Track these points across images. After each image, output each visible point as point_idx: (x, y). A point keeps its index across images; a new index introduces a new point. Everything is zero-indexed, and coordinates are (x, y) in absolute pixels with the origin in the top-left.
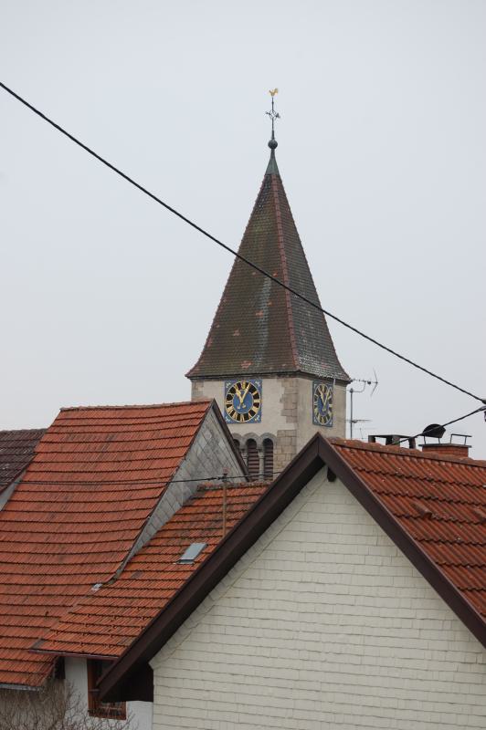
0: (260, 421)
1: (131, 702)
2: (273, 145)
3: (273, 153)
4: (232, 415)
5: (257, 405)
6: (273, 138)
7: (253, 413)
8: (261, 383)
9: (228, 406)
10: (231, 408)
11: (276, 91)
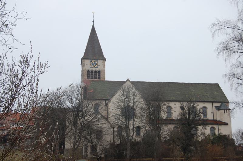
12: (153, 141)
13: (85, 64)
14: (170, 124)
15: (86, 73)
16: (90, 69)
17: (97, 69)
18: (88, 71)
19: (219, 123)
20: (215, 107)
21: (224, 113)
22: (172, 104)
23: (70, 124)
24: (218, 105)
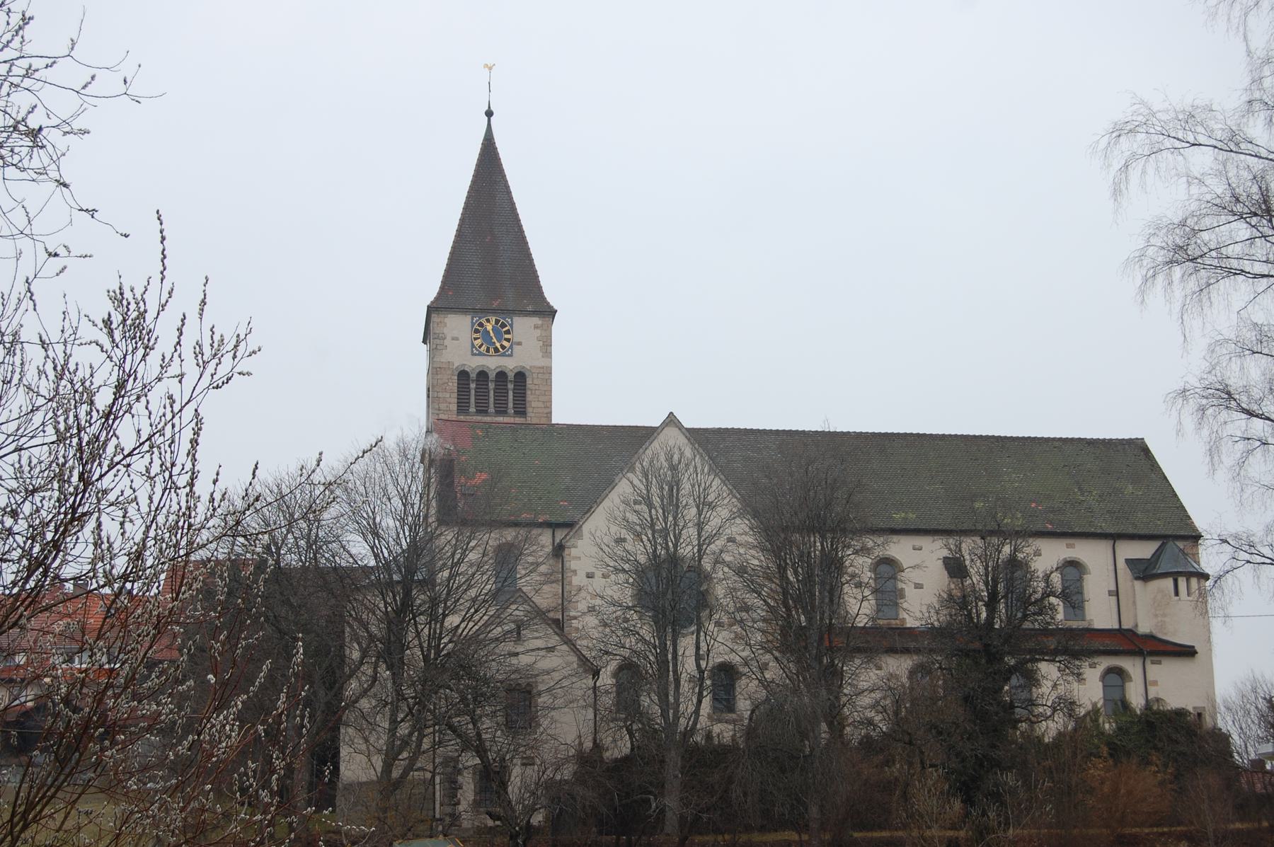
0: (473, 354)
1: (1109, 627)
2: (489, 114)
3: (489, 121)
4: (480, 347)
5: (508, 340)
6: (489, 107)
7: (503, 347)
8: (512, 321)
9: (475, 339)
10: (479, 340)
11: (486, 66)
15: (453, 385)
16: (475, 364)
18: (463, 375)
20: (1129, 562)
21: (1177, 594)
22: (901, 549)
23: (364, 653)
24: (1144, 550)
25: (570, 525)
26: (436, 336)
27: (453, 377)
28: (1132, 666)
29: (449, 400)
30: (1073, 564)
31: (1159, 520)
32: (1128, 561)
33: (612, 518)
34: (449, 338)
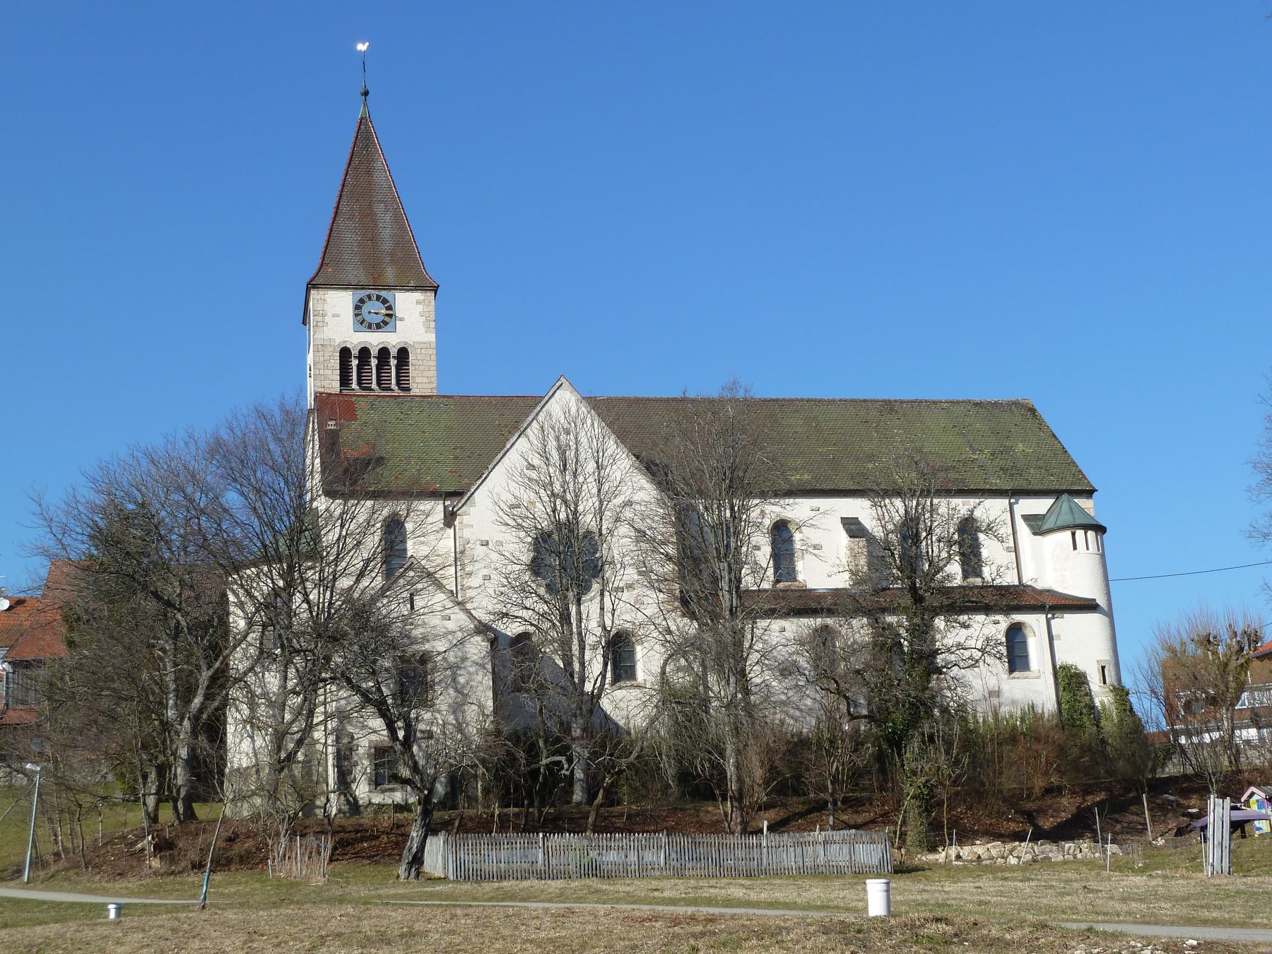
12: (276, 598)
13: (323, 316)
14: (987, 609)
15: (335, 362)
16: (357, 340)
17: (391, 339)
18: (345, 353)
19: (1049, 603)
20: (1026, 518)
21: (1075, 548)
22: (798, 509)
23: (250, 623)
24: (1040, 506)
25: (458, 494)
26: (316, 313)
27: (335, 354)
28: (1034, 622)
29: (331, 377)
30: (826, 628)
31: (1052, 475)
32: (1023, 516)
33: (511, 476)
34: (330, 315)
